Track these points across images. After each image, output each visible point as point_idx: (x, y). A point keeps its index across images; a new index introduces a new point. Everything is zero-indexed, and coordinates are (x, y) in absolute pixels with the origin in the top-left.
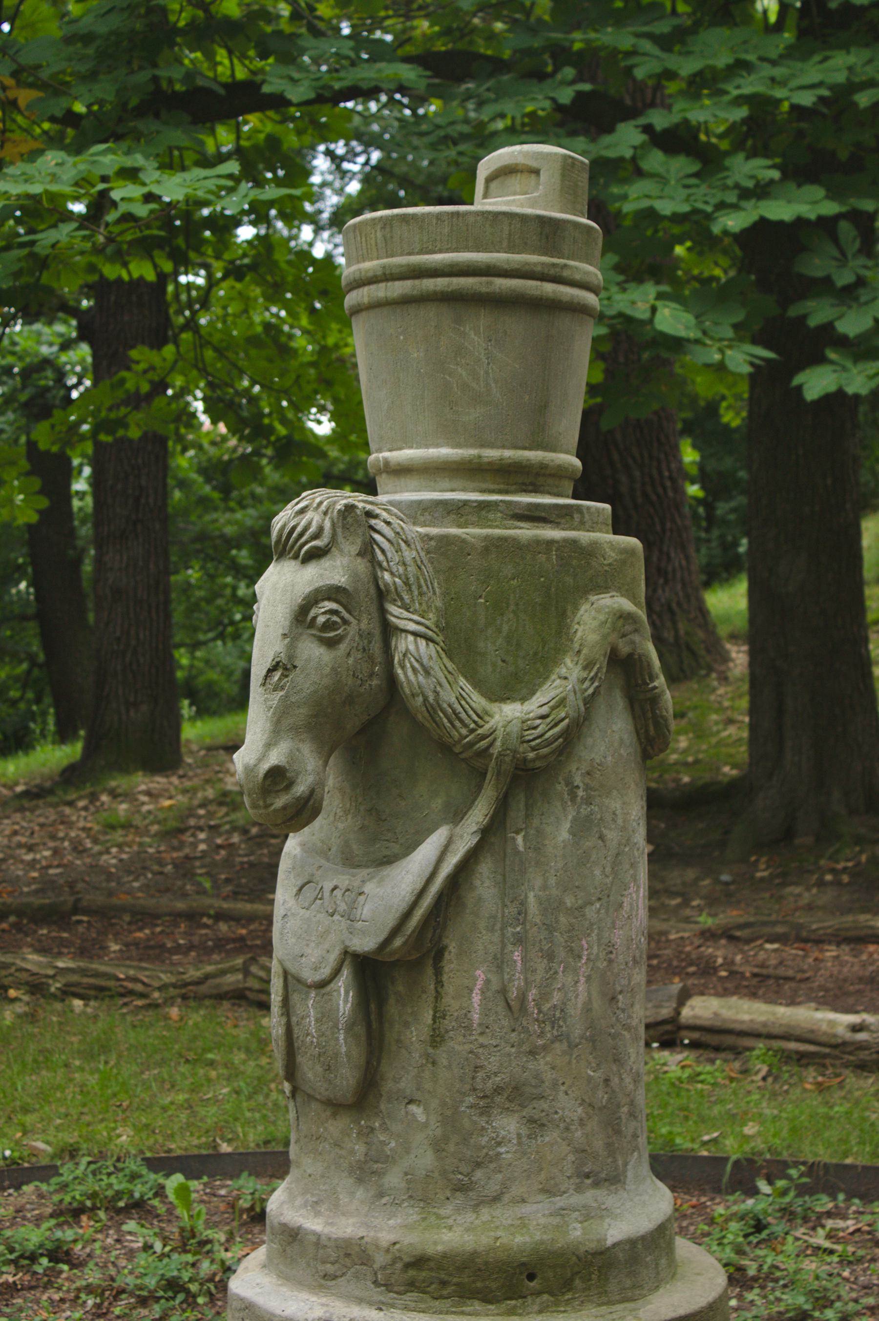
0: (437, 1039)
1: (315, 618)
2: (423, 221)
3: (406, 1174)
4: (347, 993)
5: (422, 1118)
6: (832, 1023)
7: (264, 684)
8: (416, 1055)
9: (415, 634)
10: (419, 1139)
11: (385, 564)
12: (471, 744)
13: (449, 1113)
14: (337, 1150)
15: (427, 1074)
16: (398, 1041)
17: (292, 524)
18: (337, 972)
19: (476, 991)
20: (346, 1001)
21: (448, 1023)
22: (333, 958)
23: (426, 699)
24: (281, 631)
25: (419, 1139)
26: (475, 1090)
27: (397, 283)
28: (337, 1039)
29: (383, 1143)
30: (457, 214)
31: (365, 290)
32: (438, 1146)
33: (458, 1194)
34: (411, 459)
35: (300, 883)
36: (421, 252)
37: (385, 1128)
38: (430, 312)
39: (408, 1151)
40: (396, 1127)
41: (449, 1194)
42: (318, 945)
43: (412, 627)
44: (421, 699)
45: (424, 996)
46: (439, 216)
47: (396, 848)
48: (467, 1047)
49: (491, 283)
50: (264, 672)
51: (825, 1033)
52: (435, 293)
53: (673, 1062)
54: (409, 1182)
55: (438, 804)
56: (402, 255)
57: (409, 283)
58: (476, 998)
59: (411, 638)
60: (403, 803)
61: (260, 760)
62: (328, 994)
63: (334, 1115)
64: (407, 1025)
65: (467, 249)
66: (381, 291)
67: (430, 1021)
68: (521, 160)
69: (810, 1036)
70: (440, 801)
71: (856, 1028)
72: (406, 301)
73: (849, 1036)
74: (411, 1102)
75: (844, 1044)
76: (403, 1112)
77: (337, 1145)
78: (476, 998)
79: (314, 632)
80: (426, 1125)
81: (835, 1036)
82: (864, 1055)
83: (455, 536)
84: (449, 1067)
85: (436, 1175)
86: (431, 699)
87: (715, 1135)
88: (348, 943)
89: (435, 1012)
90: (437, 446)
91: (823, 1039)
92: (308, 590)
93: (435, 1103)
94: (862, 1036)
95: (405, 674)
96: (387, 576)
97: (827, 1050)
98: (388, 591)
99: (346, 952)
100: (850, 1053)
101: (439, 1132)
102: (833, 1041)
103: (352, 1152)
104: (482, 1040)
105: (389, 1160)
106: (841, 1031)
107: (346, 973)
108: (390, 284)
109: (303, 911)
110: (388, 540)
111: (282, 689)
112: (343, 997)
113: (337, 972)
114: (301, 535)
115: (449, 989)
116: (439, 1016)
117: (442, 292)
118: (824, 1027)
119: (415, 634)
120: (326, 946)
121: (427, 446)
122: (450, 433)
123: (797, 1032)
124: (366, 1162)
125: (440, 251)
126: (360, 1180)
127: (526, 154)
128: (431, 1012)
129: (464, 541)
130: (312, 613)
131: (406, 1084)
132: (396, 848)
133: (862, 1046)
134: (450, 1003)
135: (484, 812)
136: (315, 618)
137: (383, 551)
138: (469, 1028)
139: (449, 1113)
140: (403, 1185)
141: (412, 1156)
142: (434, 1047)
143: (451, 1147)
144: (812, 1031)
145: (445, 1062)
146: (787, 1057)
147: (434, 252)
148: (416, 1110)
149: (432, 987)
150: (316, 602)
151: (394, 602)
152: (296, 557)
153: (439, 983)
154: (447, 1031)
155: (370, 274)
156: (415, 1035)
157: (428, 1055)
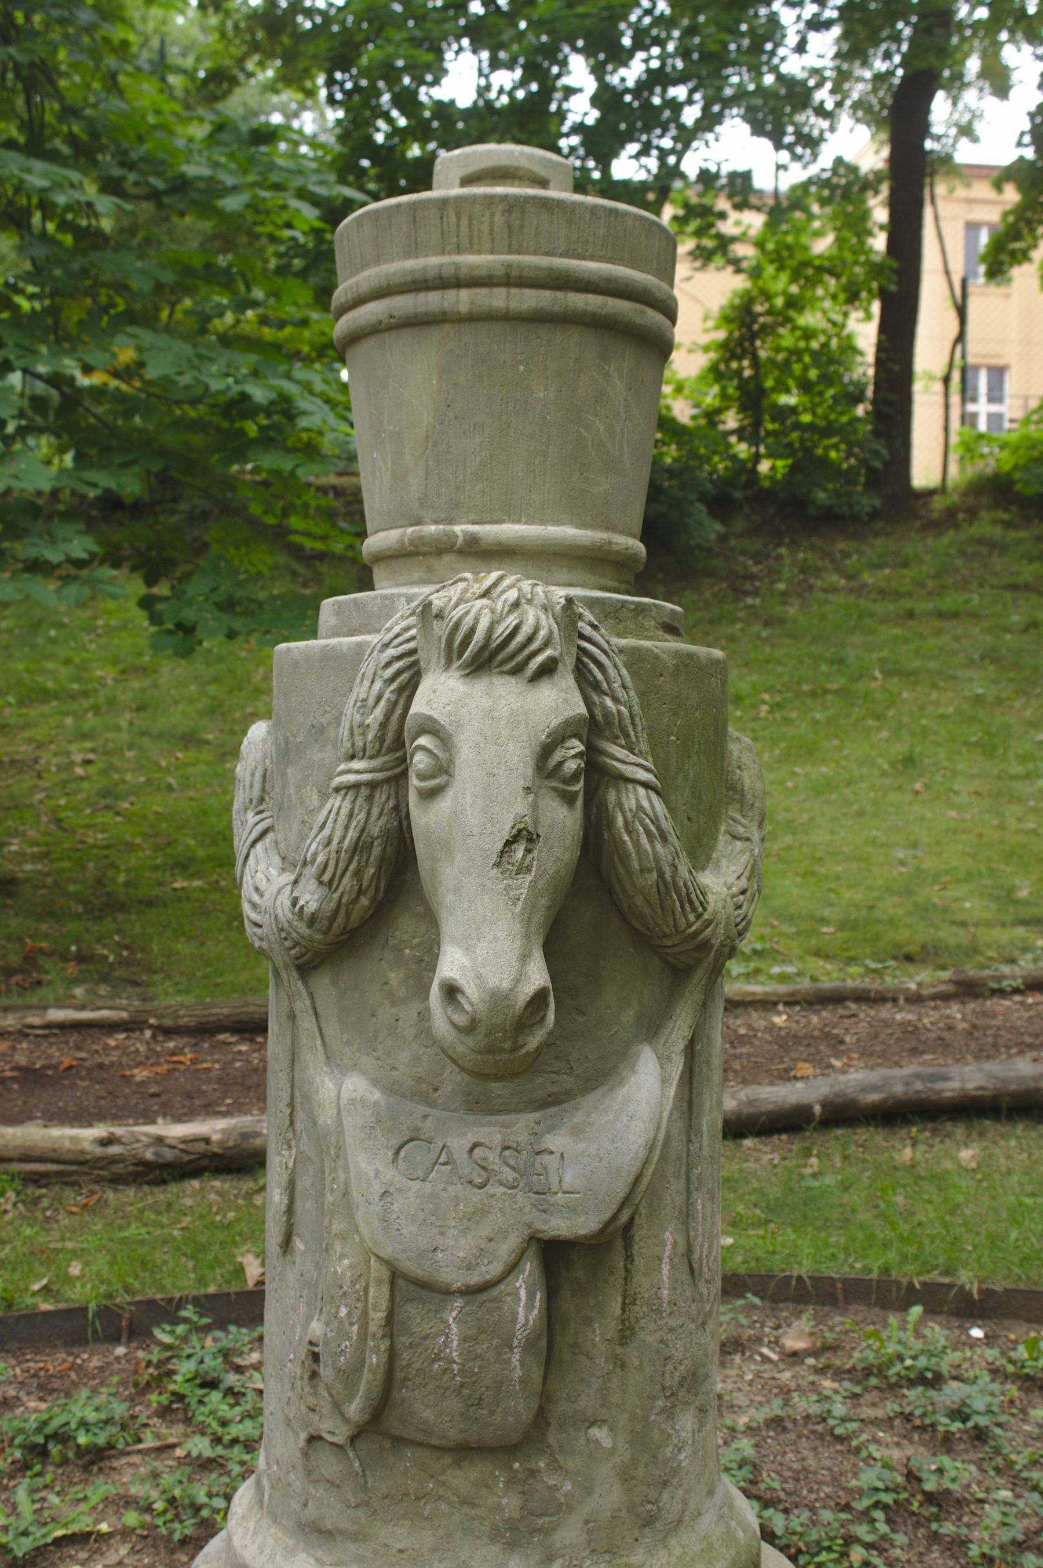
0: (626, 1333)
1: (561, 764)
2: (573, 211)
3: (587, 1522)
4: (531, 1296)
5: (607, 1443)
6: (74, 1139)
7: (497, 865)
8: (601, 1361)
9: (646, 785)
10: (605, 1473)
11: (605, 685)
12: (697, 933)
13: (638, 1427)
14: (466, 1509)
15: (615, 1383)
16: (575, 1345)
17: (512, 620)
18: (512, 1268)
19: (666, 1260)
20: (530, 1306)
21: (639, 1309)
22: (506, 1250)
23: (661, 874)
24: (521, 783)
25: (605, 1473)
26: (664, 1388)
27: (527, 292)
28: (508, 1362)
29: (555, 1488)
30: (615, 212)
31: (464, 294)
32: (626, 1476)
33: (647, 1530)
34: (523, 538)
35: (395, 1142)
36: (565, 254)
37: (555, 1466)
38: (572, 339)
39: (589, 1492)
40: (572, 1463)
41: (636, 1533)
42: (464, 1232)
43: (643, 775)
44: (655, 875)
45: (612, 1279)
46: (594, 209)
47: (568, 1082)
48: (658, 1335)
49: (643, 312)
50: (499, 846)
51: (69, 1151)
52: (585, 313)
53: (299, 1244)
54: (590, 1532)
55: (629, 1016)
56: (536, 253)
57: (547, 294)
58: (666, 1268)
59: (642, 791)
60: (581, 1019)
61: (517, 981)
62: (497, 1299)
63: (458, 1464)
64: (588, 1322)
65: (621, 262)
66: (498, 299)
67: (618, 1312)
68: (524, 163)
69: (52, 1155)
70: (632, 1013)
71: (107, 1142)
72: (474, 318)
73: (99, 1151)
74: (592, 1424)
75: (98, 1159)
76: (582, 1441)
77: (467, 1502)
78: (666, 1268)
79: (555, 784)
80: (612, 1451)
81: (82, 1152)
82: (118, 1168)
83: (648, 650)
84: (640, 1368)
85: (624, 1513)
86: (668, 876)
87: (45, 1281)
88: (539, 1226)
89: (624, 1298)
90: (558, 523)
91: (70, 1157)
92: (555, 722)
93: (623, 1420)
94: (115, 1150)
95: (637, 843)
96: (609, 702)
97: (74, 1168)
98: (609, 724)
99: (534, 1239)
100: (101, 1168)
101: (627, 1456)
102: (81, 1158)
103: (498, 1508)
104: (672, 1322)
105: (562, 1509)
106: (87, 1146)
107: (529, 1267)
108: (514, 291)
109: (416, 1185)
110: (604, 652)
111: (528, 870)
112: (524, 1304)
113: (512, 1268)
114: (530, 639)
115: (640, 1263)
116: (628, 1301)
117: (594, 314)
118: (67, 1144)
119: (646, 785)
120: (486, 1231)
121: (543, 522)
122: (578, 508)
123: (37, 1153)
124: (522, 1518)
125: (592, 258)
126: (512, 1545)
127: (531, 158)
128: (620, 1299)
129: (656, 657)
130: (557, 756)
131: (587, 1402)
132: (568, 1082)
133: (114, 1160)
134: (641, 1281)
135: (689, 1022)
136: (561, 764)
137: (600, 666)
138: (658, 1311)
139: (638, 1427)
140: (584, 1537)
141: (595, 1496)
142: (622, 1345)
143: (641, 1472)
144: (54, 1150)
145: (636, 1362)
146: (37, 1179)
147: (584, 258)
148: (600, 1434)
149: (621, 1265)
150: (563, 740)
151: (614, 739)
152: (517, 671)
153: (629, 1258)
154: (637, 1320)
155: (483, 272)
156: (600, 1335)
157: (616, 1356)
